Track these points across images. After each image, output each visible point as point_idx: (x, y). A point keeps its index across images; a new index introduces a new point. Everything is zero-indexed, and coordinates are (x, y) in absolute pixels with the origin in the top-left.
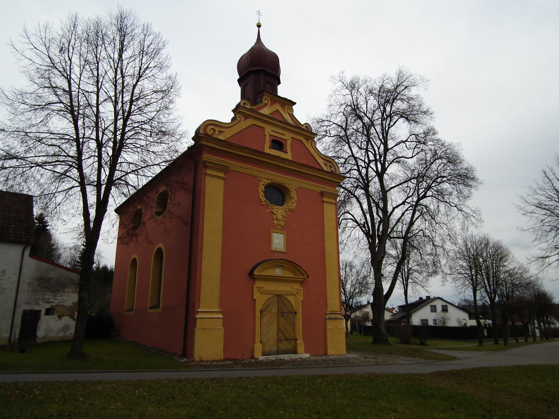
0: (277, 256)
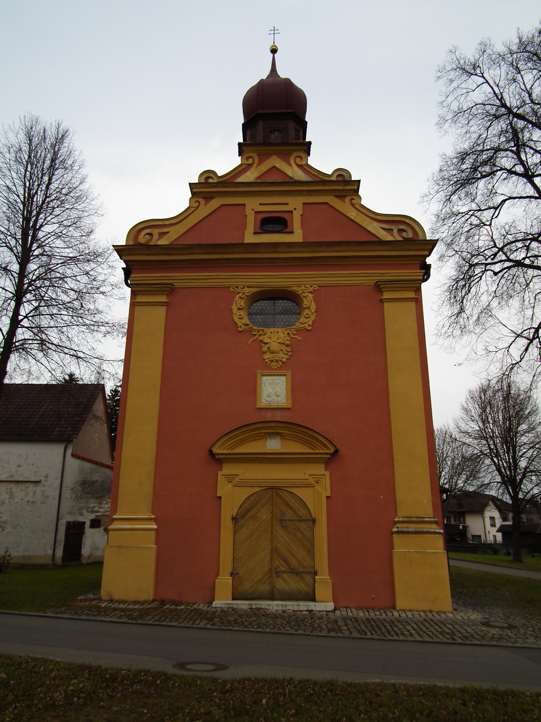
0: (269, 416)
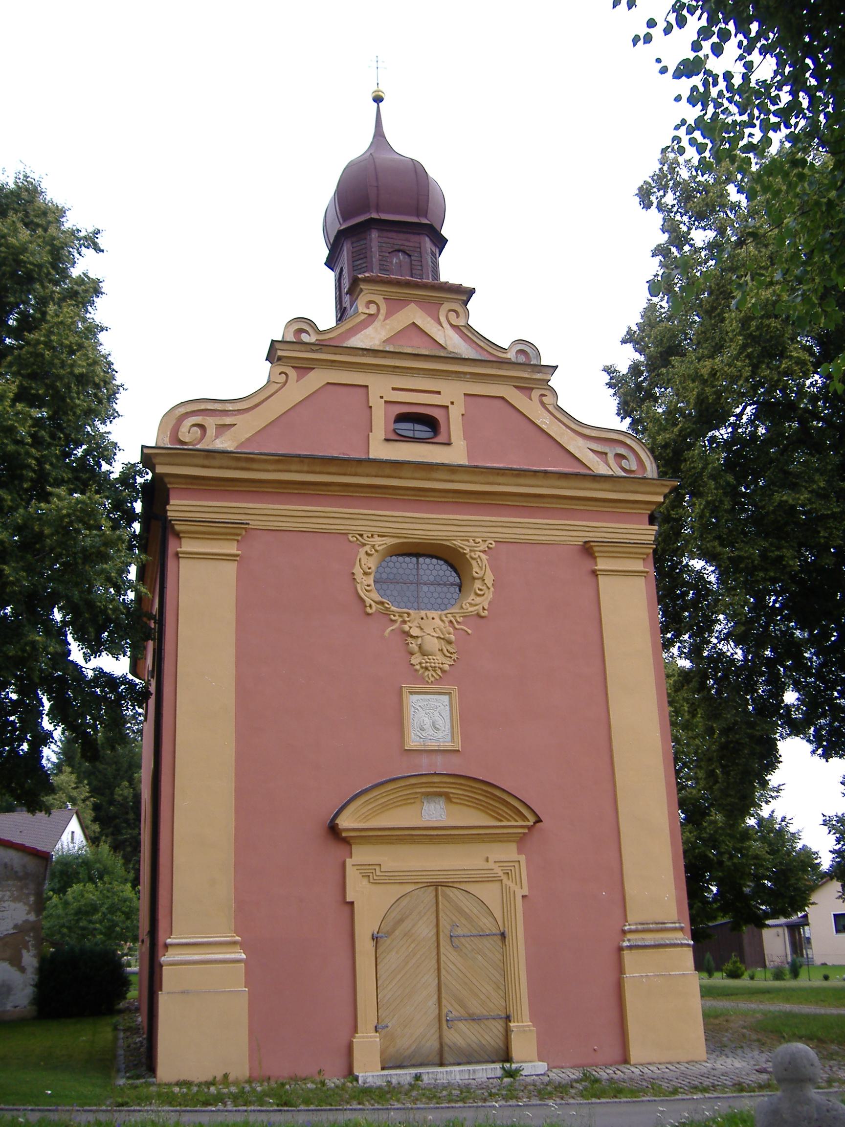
0: (425, 765)
